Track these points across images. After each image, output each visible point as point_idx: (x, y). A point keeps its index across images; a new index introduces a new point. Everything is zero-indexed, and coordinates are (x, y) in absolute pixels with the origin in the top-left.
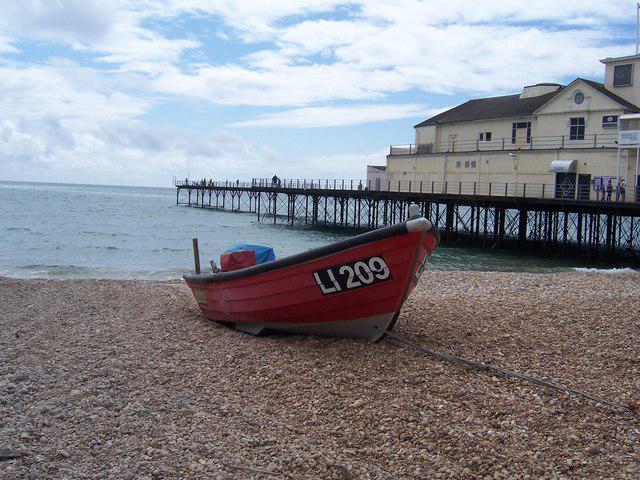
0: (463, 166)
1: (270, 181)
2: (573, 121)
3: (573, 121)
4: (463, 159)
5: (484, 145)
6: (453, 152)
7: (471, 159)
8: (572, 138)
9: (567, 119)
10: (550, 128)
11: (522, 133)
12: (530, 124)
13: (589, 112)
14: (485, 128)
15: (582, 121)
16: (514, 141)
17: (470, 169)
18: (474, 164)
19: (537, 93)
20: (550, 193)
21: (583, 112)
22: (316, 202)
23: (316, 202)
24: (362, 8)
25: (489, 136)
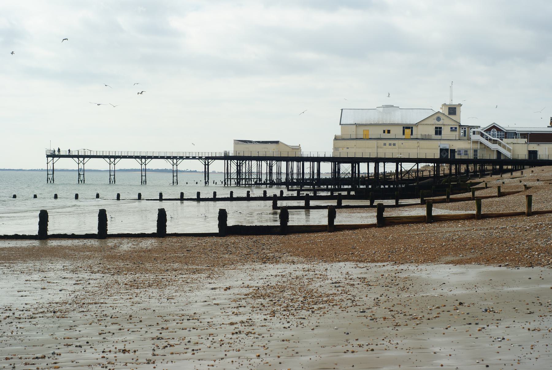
0: (387, 145)
2: (436, 128)
3: (436, 128)
4: (388, 142)
5: (387, 135)
7: (392, 142)
8: (441, 128)
13: (444, 125)
15: (441, 128)
20: (438, 156)
25: (389, 132)
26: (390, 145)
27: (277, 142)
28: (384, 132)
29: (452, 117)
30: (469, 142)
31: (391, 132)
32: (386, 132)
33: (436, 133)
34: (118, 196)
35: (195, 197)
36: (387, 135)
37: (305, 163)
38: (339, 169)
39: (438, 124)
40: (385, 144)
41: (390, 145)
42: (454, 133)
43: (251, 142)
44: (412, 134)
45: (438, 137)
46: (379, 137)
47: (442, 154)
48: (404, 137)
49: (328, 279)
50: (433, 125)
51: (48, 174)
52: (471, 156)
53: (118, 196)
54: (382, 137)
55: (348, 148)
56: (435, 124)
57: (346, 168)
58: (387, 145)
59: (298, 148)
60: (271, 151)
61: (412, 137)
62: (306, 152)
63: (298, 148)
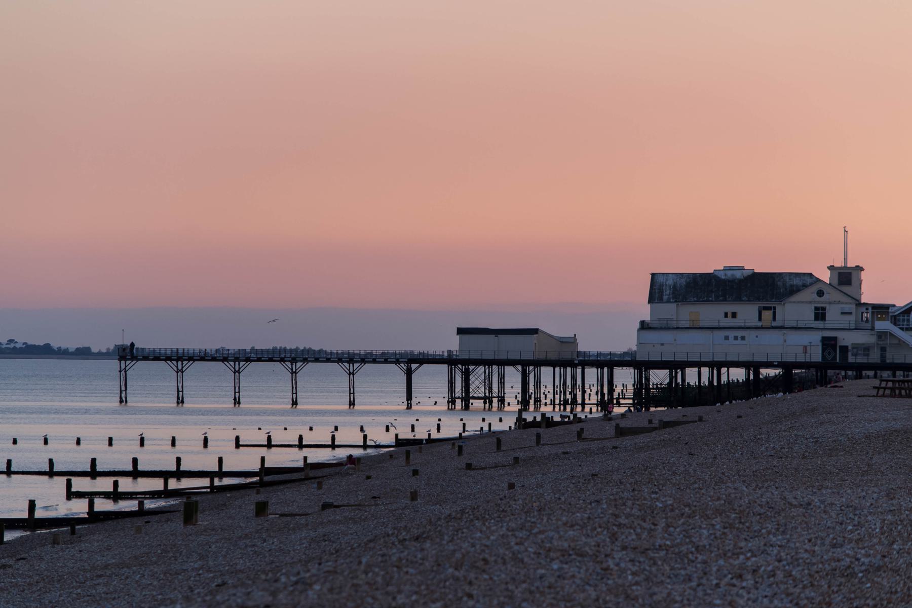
0: (731, 339)
1: (446, 354)
2: (816, 309)
3: (816, 309)
4: (731, 334)
5: (730, 322)
6: (294, 361)
7: (739, 334)
8: (824, 309)
9: (813, 307)
10: (795, 311)
11: (767, 315)
12: (775, 308)
13: (830, 303)
14: (730, 308)
15: (824, 309)
16: (850, 313)
17: (739, 341)
18: (743, 338)
19: (797, 282)
21: (826, 303)
22: (466, 376)
23: (466, 376)
24: (851, 264)
25: (734, 315)
26: (736, 338)
27: (535, 331)
28: (726, 315)
29: (845, 289)
30: (873, 332)
31: (738, 315)
32: (730, 315)
33: (817, 318)
34: (110, 444)
35: (88, 468)
36: (730, 322)
37: (617, 371)
38: (648, 379)
39: (819, 302)
40: (727, 338)
41: (736, 338)
42: (847, 318)
43: (45, 351)
44: (774, 319)
45: (820, 324)
46: (716, 325)
47: (826, 353)
48: (759, 324)
49: (725, 576)
50: (810, 302)
51: (411, 362)
52: (875, 357)
53: (110, 444)
54: (721, 325)
55: (662, 344)
56: (815, 302)
57: (659, 377)
58: (731, 339)
59: (572, 341)
60: (525, 348)
61: (774, 324)
62: (587, 345)
63: (572, 341)
